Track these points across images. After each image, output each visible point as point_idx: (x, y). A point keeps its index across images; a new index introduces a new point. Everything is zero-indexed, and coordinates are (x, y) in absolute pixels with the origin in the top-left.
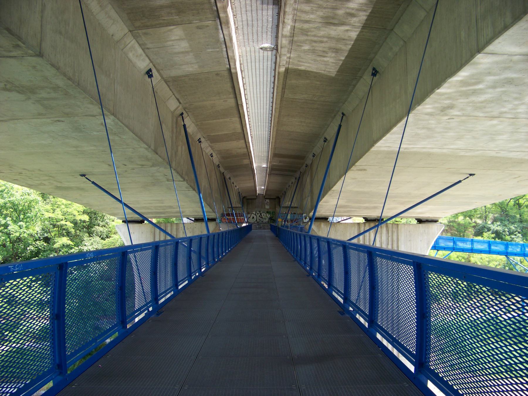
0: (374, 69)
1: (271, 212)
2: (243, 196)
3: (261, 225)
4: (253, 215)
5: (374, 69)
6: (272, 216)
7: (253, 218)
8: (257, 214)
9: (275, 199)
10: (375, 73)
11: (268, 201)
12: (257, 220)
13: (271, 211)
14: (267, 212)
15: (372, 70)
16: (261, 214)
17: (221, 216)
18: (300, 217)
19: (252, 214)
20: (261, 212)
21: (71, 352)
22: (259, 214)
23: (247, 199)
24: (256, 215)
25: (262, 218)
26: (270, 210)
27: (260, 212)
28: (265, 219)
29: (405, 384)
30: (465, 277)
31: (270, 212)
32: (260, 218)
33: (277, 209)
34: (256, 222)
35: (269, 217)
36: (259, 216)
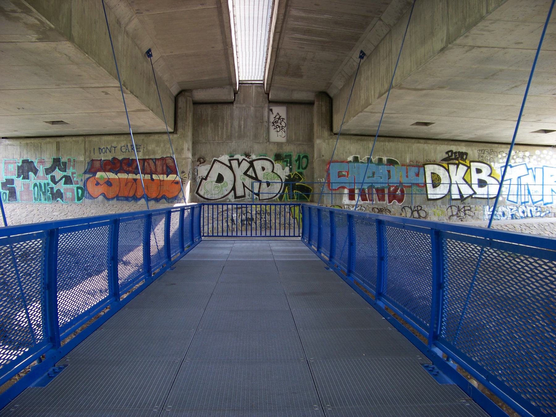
0: (362, 52)
1: (294, 158)
3: (254, 210)
4: (218, 169)
5: (362, 52)
6: (295, 171)
7: (220, 179)
8: (235, 164)
9: (311, 104)
11: (280, 111)
12: (234, 189)
13: (293, 150)
14: (278, 157)
15: (360, 53)
16: (251, 163)
17: (85, 173)
18: (413, 179)
19: (217, 165)
20: (254, 157)
21: (18, 355)
22: (245, 165)
23: (195, 103)
24: (231, 168)
25: (256, 179)
26: (287, 149)
27: (248, 155)
28: (268, 184)
29: (418, 357)
30: (490, 244)
31: (290, 156)
32: (248, 182)
33: (318, 142)
34: (231, 196)
35: (284, 177)
36: (245, 173)
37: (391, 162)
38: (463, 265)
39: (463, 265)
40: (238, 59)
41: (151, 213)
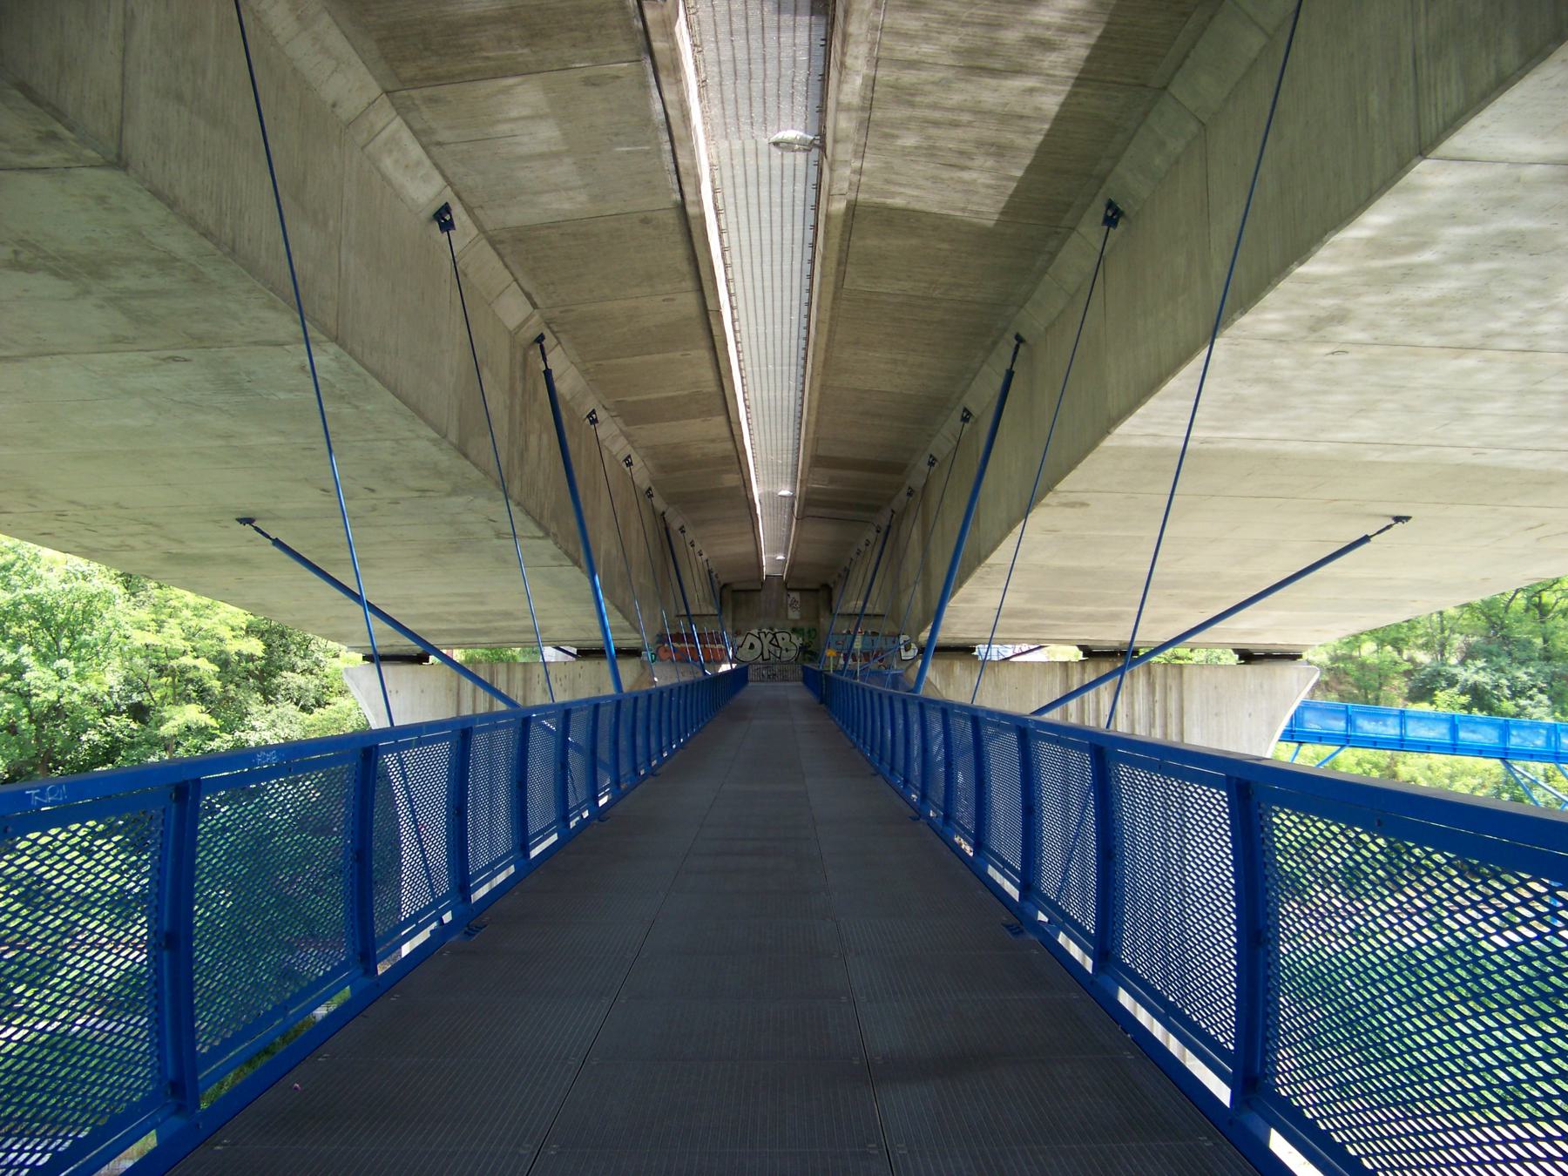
0: (1110, 205)
1: (806, 630)
3: (776, 668)
4: (750, 639)
5: (1110, 205)
6: (807, 641)
7: (752, 646)
8: (762, 635)
9: (817, 591)
10: (1113, 216)
11: (795, 596)
12: (762, 654)
13: (805, 625)
14: (794, 630)
15: (1104, 209)
16: (774, 635)
17: (657, 643)
18: (890, 645)
19: (749, 637)
20: (776, 630)
21: (210, 1044)
22: (770, 636)
23: (734, 591)
24: (759, 638)
25: (778, 646)
26: (801, 625)
27: (772, 629)
28: (787, 650)
29: (1203, 1141)
31: (803, 630)
32: (772, 648)
33: (822, 620)
34: (760, 659)
35: (798, 645)
36: (770, 642)
37: (874, 634)
38: (1346, 910)
39: (1346, 910)
40: (735, 311)
41: (469, 726)
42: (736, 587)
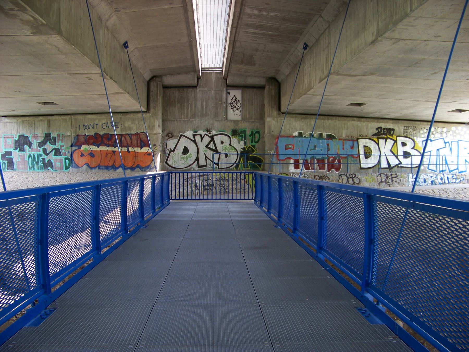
0: (305, 44)
1: (248, 133)
2: (147, 77)
3: (214, 177)
4: (184, 143)
5: (305, 44)
6: (249, 145)
7: (186, 151)
8: (198, 138)
10: (306, 47)
11: (236, 94)
12: (197, 159)
13: (247, 127)
14: (235, 133)
15: (303, 45)
16: (212, 138)
17: (72, 146)
18: (348, 151)
19: (183, 139)
20: (214, 132)
21: (15, 300)
22: (207, 139)
23: (165, 87)
24: (195, 142)
25: (216, 151)
26: (242, 126)
27: (209, 131)
28: (226, 155)
29: (353, 302)
31: (244, 132)
32: (209, 153)
33: (268, 120)
34: (195, 166)
35: (239, 150)
36: (207, 146)
37: (330, 137)
42: (169, 80)
